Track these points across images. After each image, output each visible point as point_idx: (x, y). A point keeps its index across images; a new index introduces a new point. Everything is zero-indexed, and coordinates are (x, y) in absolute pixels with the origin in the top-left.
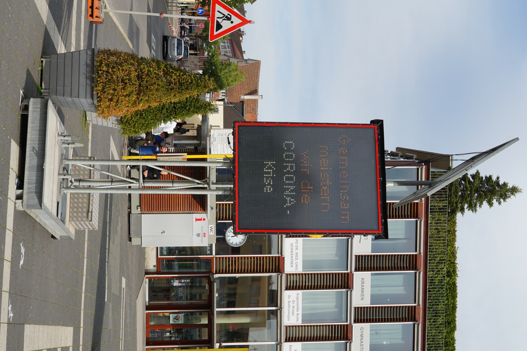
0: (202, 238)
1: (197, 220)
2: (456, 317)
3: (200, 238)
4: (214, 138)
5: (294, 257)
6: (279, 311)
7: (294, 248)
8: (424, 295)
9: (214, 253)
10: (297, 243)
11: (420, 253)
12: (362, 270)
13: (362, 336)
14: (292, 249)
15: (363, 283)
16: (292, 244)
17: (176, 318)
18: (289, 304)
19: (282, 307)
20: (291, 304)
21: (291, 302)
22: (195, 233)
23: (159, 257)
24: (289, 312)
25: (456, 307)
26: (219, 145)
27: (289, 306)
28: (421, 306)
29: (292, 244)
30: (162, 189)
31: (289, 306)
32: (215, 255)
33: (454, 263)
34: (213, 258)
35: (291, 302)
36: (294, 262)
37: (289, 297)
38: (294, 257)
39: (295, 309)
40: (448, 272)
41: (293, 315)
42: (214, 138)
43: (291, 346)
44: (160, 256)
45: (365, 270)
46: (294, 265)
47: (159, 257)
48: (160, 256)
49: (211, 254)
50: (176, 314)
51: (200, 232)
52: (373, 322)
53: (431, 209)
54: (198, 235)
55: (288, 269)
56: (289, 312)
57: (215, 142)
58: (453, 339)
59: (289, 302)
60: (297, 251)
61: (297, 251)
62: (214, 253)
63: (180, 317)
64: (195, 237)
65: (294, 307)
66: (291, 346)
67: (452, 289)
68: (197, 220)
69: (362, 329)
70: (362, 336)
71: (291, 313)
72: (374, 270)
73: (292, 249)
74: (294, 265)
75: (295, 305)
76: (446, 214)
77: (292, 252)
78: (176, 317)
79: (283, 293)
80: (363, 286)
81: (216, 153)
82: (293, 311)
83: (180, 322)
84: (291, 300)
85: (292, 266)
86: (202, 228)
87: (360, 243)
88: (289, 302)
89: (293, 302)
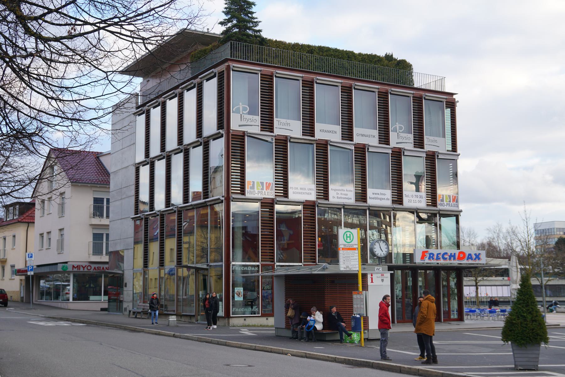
0: (384, 277)
1: (372, 282)
2: (276, 40)
3: (385, 279)
4: (347, 268)
5: (304, 191)
6: (346, 207)
7: (296, 191)
8: (331, 77)
9: (257, 264)
10: (407, 196)
11: (261, 71)
12: (314, 131)
13: (363, 135)
14: (297, 193)
15: (323, 131)
16: (294, 193)
17: (239, 295)
18: (339, 198)
19: (343, 204)
20: (339, 196)
21: (338, 195)
22: (381, 283)
23: (260, 315)
24: (345, 198)
25: (336, 49)
26: (352, 263)
27: (341, 198)
28: (304, 75)
29: (294, 193)
30: (111, 314)
31: (341, 198)
32: (302, 263)
33: (294, 44)
34: (261, 264)
35: (338, 195)
36: (308, 192)
37: (334, 197)
38: (304, 191)
39: (343, 192)
40: (308, 52)
41: (347, 195)
42: (347, 268)
43: (370, 198)
44: (232, 315)
45: (389, 137)
46: (310, 191)
47: (260, 315)
48: (232, 315)
49: (258, 266)
50: (234, 295)
51: (380, 279)
52: (314, 120)
53: (257, 61)
54: (383, 280)
55: (312, 197)
56: (345, 198)
57: (350, 267)
58: (360, 54)
59: (338, 198)
60: (299, 188)
61: (299, 188)
62: (257, 264)
63: (237, 291)
64: (384, 283)
65: (341, 194)
66: (370, 198)
67: (322, 50)
68: (372, 282)
69: (358, 135)
70: (363, 135)
71: (347, 197)
72: (273, 115)
73: (297, 193)
74: (310, 191)
75: (339, 192)
76: (264, 48)
77: (300, 193)
78: (237, 295)
79: (290, 200)
80: (326, 131)
81: (357, 266)
82: (344, 194)
83: (242, 291)
84: (336, 196)
85: (311, 194)
86: (377, 277)
87: (292, 131)
88: (338, 198)
89: (338, 194)
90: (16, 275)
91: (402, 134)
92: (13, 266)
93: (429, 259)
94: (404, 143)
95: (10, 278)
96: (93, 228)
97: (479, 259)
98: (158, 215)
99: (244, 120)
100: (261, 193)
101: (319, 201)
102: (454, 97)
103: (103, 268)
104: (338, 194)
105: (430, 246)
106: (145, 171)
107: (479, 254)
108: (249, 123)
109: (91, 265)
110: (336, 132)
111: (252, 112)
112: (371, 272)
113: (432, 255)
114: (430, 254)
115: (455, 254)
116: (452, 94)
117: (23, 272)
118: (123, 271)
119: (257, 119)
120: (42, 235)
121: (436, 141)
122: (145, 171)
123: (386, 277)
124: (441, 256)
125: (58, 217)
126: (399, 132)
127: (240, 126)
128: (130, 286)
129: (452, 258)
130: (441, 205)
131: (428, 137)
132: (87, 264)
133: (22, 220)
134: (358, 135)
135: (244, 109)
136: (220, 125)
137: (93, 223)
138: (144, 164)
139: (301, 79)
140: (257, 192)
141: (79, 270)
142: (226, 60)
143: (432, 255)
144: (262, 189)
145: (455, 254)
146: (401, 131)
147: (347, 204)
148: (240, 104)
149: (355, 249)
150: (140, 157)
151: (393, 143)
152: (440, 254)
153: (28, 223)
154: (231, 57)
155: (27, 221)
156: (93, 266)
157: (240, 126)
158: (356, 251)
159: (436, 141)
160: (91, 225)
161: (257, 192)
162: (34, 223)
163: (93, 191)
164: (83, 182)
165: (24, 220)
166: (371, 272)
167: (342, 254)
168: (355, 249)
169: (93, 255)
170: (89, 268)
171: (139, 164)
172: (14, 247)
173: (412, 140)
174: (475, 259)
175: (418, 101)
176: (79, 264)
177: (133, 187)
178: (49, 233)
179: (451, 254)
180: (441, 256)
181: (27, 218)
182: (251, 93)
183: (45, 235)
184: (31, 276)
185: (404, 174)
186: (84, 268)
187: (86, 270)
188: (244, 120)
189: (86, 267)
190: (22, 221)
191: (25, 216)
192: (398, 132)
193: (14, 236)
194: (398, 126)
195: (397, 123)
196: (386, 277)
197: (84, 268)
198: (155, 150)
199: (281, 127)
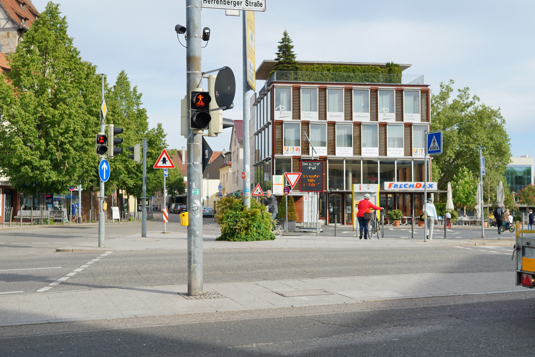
13: (359, 117)
15: (332, 116)
21: (342, 152)
24: (347, 154)
27: (343, 154)
31: (343, 154)
36: (322, 151)
37: (339, 153)
39: (345, 150)
41: (347, 152)
46: (323, 151)
59: (341, 153)
66: (363, 153)
69: (355, 117)
70: (359, 117)
74: (323, 151)
75: (343, 150)
88: (341, 153)
91: (283, 112)
93: (395, 187)
97: (432, 187)
100: (293, 153)
102: (429, 87)
104: (341, 151)
107: (432, 185)
108: (389, 118)
110: (340, 116)
111: (391, 111)
113: (396, 186)
114: (395, 185)
115: (413, 185)
116: (427, 86)
119: (394, 115)
121: (413, 116)
124: (403, 186)
129: (411, 187)
130: (415, 155)
135: (386, 110)
140: (290, 152)
143: (396, 186)
144: (294, 151)
145: (413, 185)
146: (386, 112)
147: (398, 158)
149: (281, 184)
151: (381, 119)
152: (402, 185)
158: (282, 185)
159: (413, 116)
161: (290, 152)
167: (274, 187)
168: (281, 184)
174: (429, 187)
175: (400, 92)
179: (411, 185)
180: (403, 186)
182: (340, 100)
184: (446, 191)
185: (388, 138)
192: (384, 112)
194: (384, 109)
195: (384, 108)
199: (408, 118)
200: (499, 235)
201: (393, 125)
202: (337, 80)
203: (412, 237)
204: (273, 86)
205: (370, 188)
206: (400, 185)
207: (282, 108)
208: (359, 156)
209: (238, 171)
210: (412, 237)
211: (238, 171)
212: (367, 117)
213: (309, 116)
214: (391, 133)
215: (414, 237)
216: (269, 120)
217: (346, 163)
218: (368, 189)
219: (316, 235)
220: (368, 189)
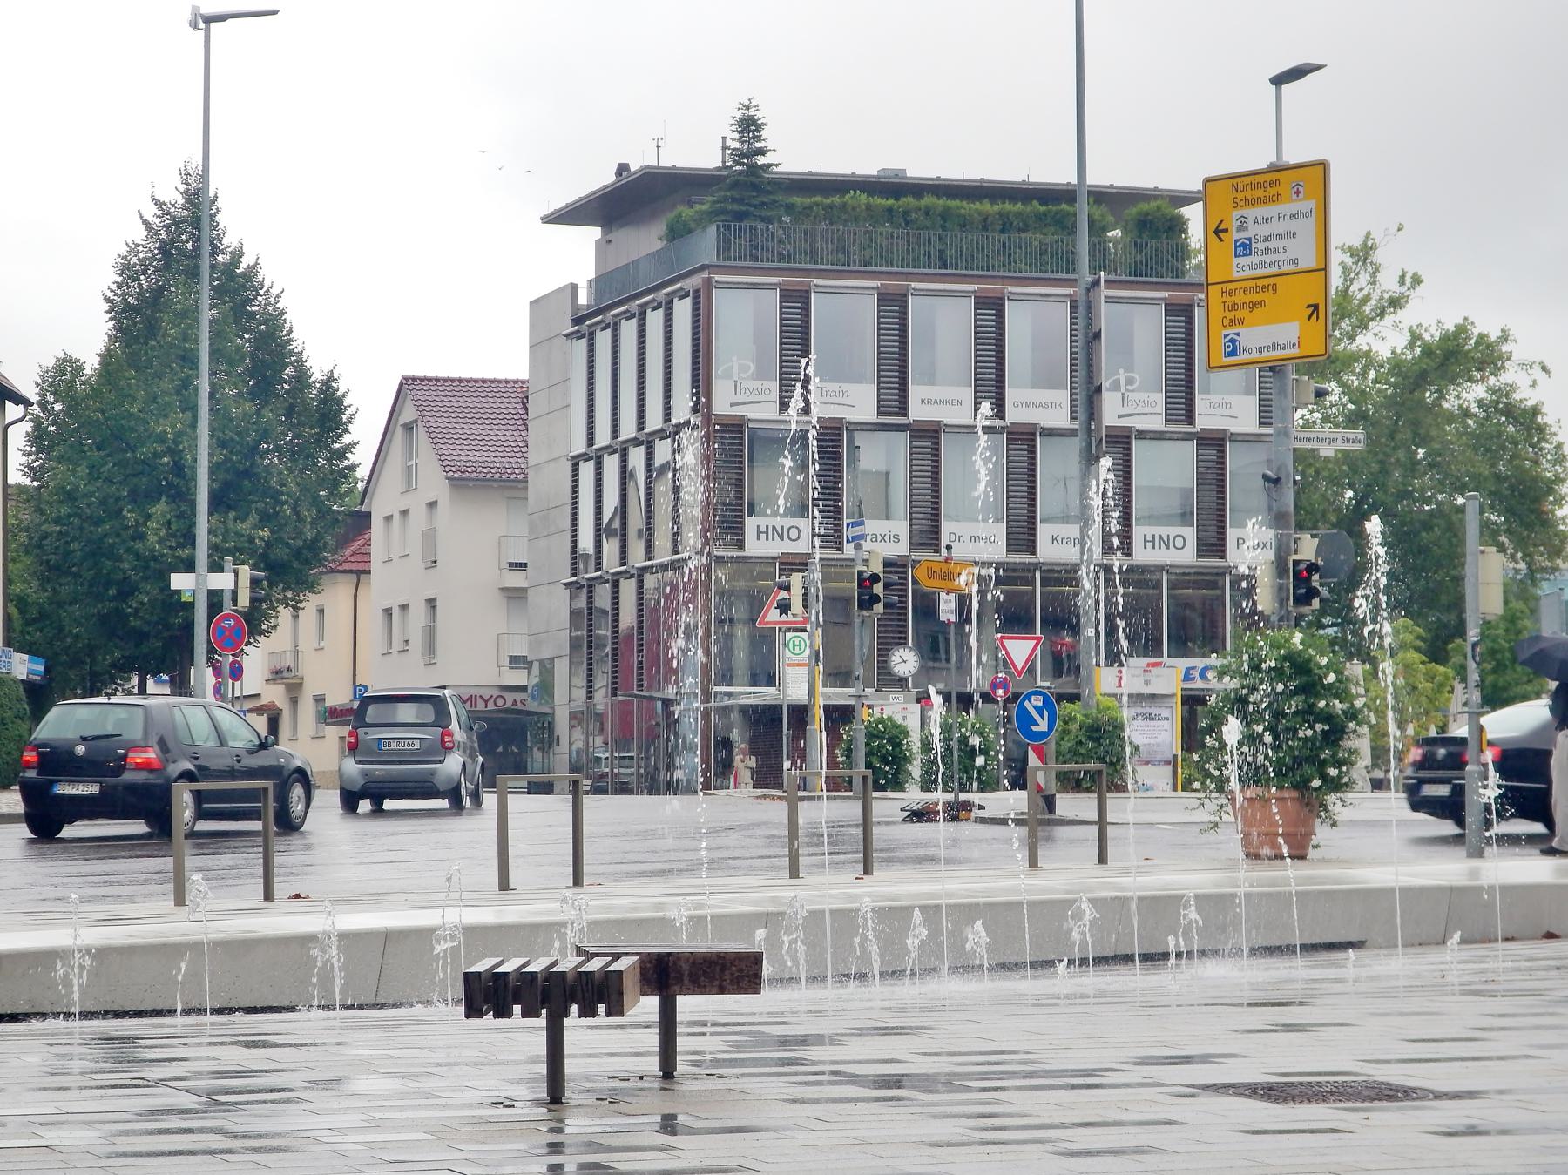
13: (1028, 405)
69: (1015, 405)
70: (1028, 405)
90: (328, 724)
91: (1132, 396)
92: (319, 699)
94: (1138, 414)
95: (313, 734)
96: (509, 598)
98: (607, 581)
99: (743, 391)
101: (915, 556)
103: (515, 702)
105: (1534, 634)
106: (587, 470)
109: (506, 695)
111: (760, 375)
112: (881, 702)
117: (342, 716)
118: (553, 708)
120: (388, 612)
121: (1228, 405)
122: (587, 470)
123: (913, 713)
124: (1196, 674)
125: (423, 566)
126: (1127, 390)
127: (732, 405)
128: (564, 741)
131: (1205, 396)
132: (496, 693)
133: (341, 564)
134: (1015, 405)
135: (743, 368)
136: (695, 410)
137: (507, 585)
138: (585, 457)
139: (876, 292)
141: (473, 709)
142: (703, 268)
148: (734, 359)
150: (580, 446)
152: (1194, 668)
153: (359, 573)
154: (718, 259)
155: (354, 567)
156: (510, 697)
157: (732, 405)
159: (1228, 405)
160: (503, 589)
162: (369, 572)
163: (509, 498)
164: (480, 476)
165: (346, 566)
166: (881, 702)
169: (510, 668)
170: (499, 702)
171: (579, 456)
172: (322, 644)
173: (1161, 408)
176: (473, 692)
177: (568, 509)
178: (404, 607)
180: (1196, 674)
181: (352, 559)
183: (396, 612)
186: (486, 702)
187: (491, 703)
188: (743, 391)
189: (493, 700)
190: (340, 568)
191: (348, 553)
192: (1123, 390)
193: (321, 611)
196: (913, 713)
197: (486, 702)
198: (603, 438)
199: (1212, 411)
200: (504, 895)
201: (1158, 436)
202: (944, 264)
203: (504, 885)
204: (708, 282)
205: (1153, 680)
206: (1188, 670)
207: (1130, 381)
208: (1027, 559)
209: (432, 603)
210: (504, 885)
211: (432, 603)
212: (1059, 405)
213: (840, 400)
214: (1054, 464)
215: (586, 880)
216: (682, 411)
217: (1044, 583)
218: (1147, 683)
219: (1532, 839)
220: (1147, 683)
